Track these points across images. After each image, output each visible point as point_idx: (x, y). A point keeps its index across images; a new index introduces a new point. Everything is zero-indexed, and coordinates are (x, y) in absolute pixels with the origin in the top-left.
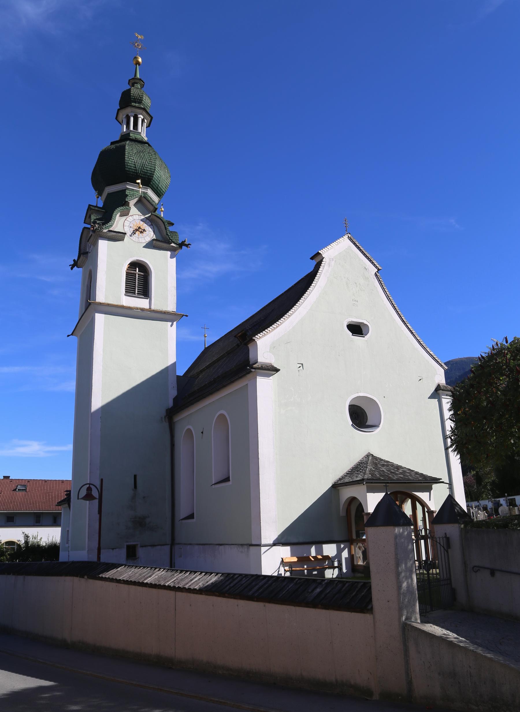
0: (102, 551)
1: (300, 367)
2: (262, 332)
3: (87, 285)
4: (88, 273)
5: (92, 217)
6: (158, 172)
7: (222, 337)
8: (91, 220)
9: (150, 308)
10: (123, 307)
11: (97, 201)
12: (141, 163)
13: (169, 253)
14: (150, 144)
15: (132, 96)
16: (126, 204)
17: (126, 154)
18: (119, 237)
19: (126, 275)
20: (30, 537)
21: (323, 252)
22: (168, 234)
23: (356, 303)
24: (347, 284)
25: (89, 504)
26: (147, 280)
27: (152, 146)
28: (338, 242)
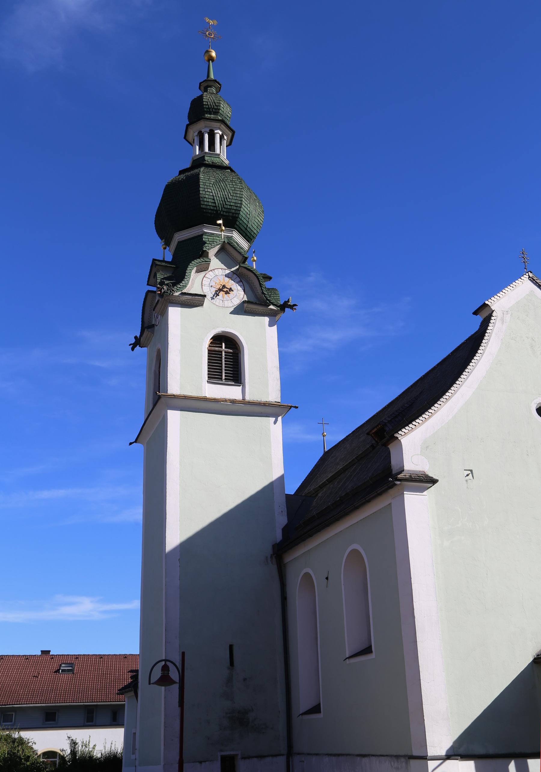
0: (185, 765)
1: (468, 475)
2: (407, 425)
3: (155, 371)
4: (155, 354)
5: (157, 276)
6: (246, 206)
7: (348, 435)
8: (157, 280)
9: (244, 399)
10: (205, 399)
11: (164, 253)
12: (222, 196)
13: (266, 319)
14: (234, 169)
15: (204, 105)
16: (204, 254)
17: (201, 186)
18: (196, 301)
19: (209, 353)
20: (79, 744)
21: (492, 302)
22: (264, 292)
24: (532, 347)
25: (165, 690)
26: (238, 359)
27: (236, 171)
28: (514, 286)
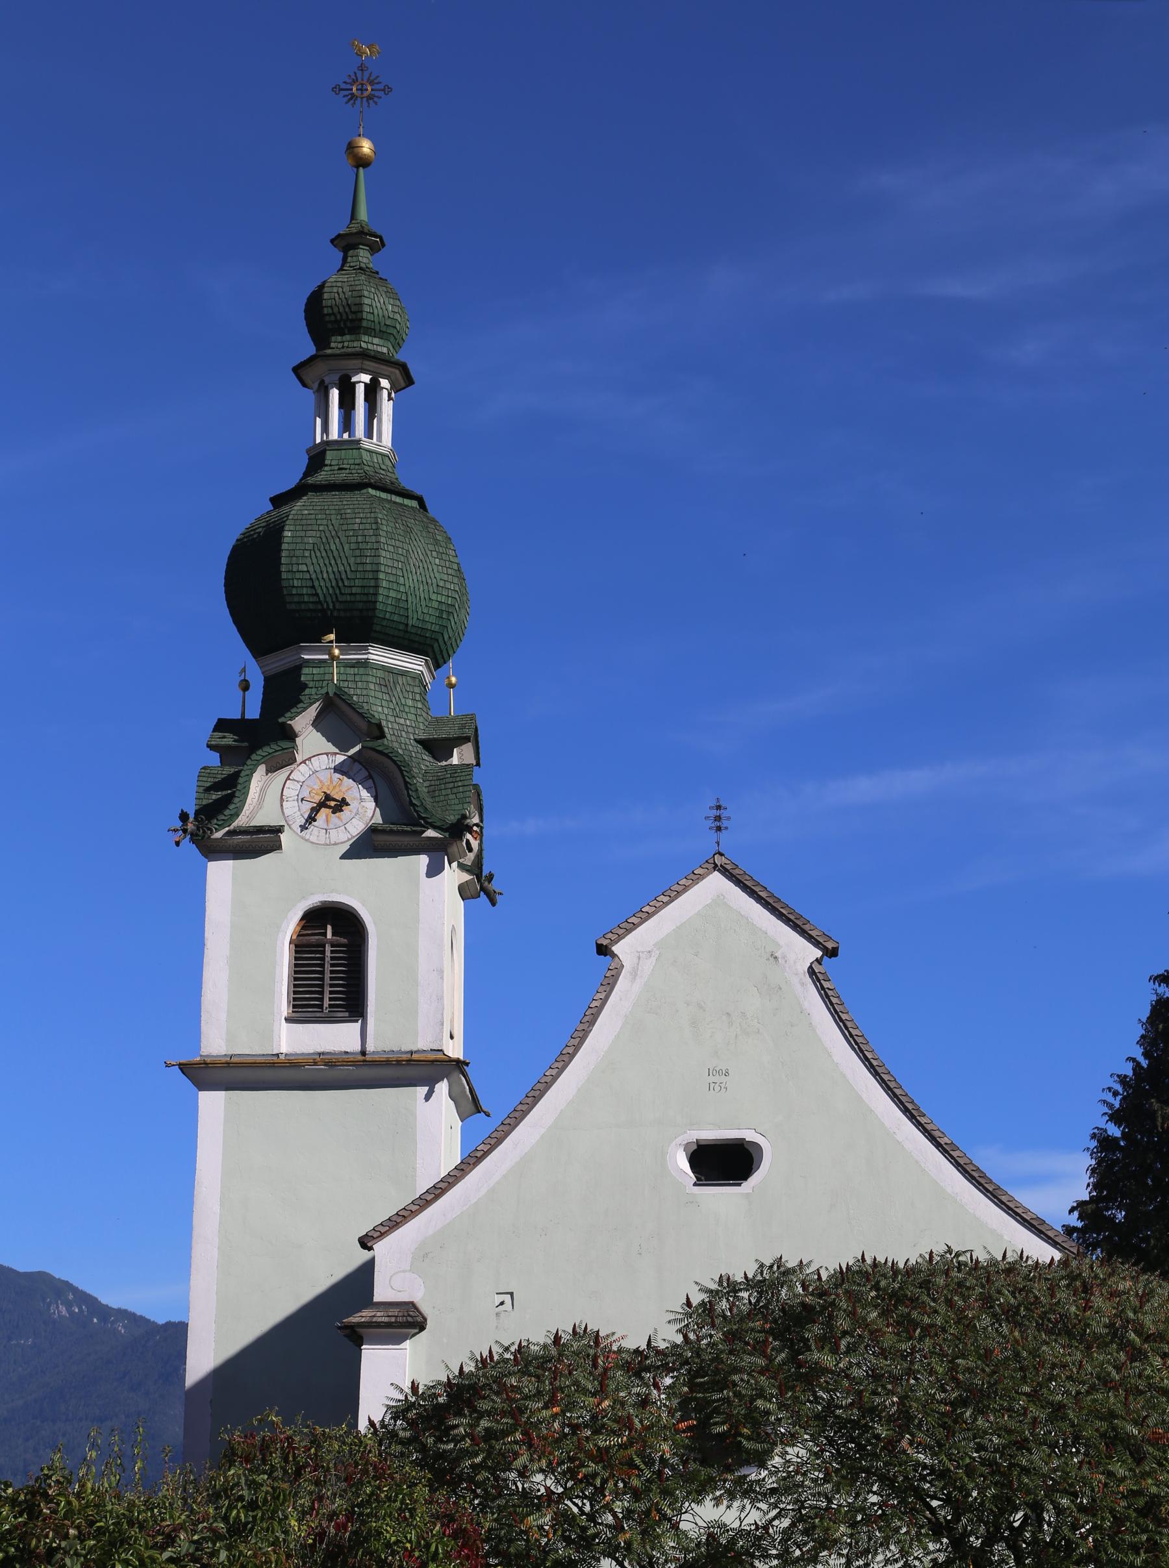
1: (502, 1303)
9: (363, 1053)
13: (423, 860)
22: (414, 801)
23: (723, 1079)
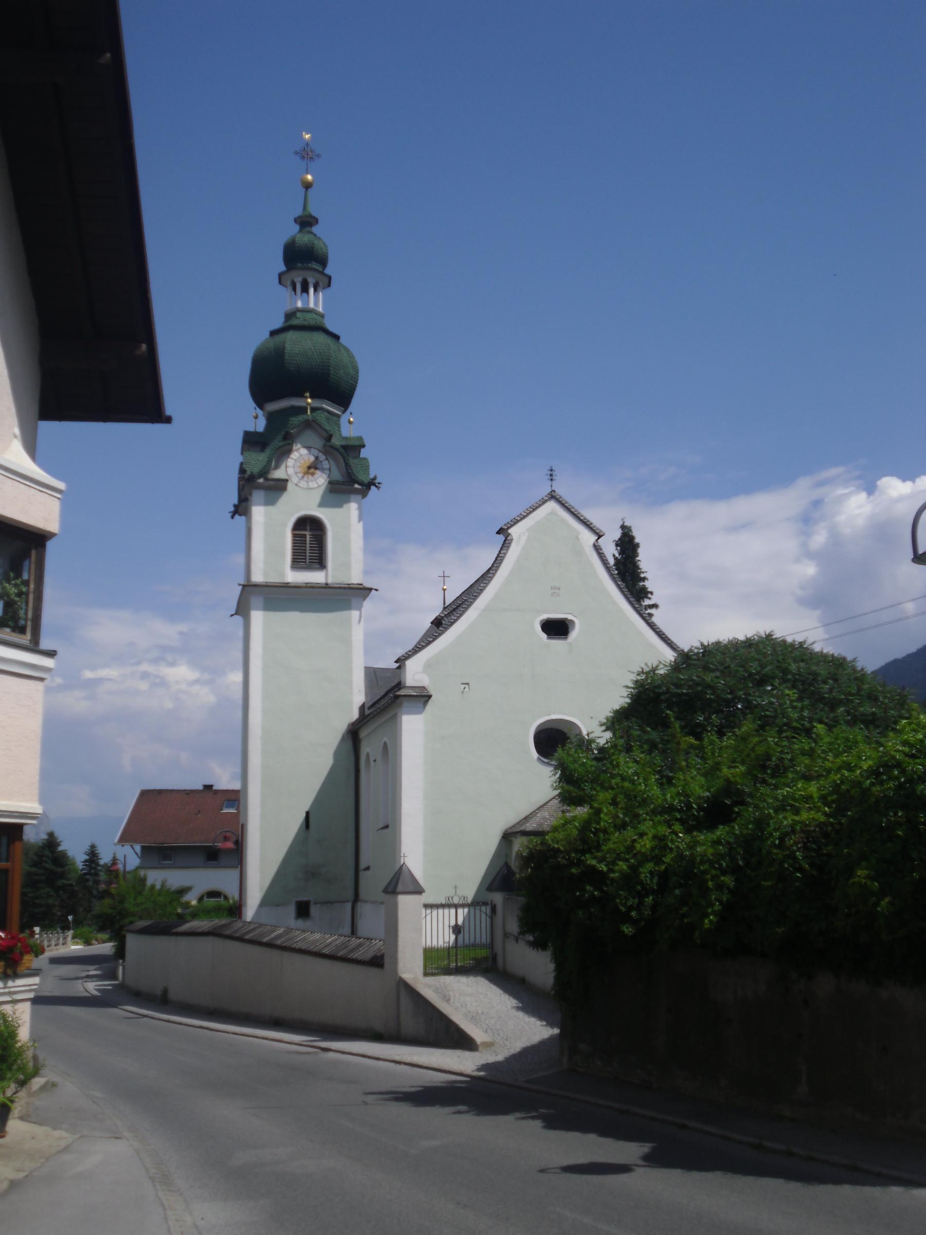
1: (465, 688)
23: (558, 591)
